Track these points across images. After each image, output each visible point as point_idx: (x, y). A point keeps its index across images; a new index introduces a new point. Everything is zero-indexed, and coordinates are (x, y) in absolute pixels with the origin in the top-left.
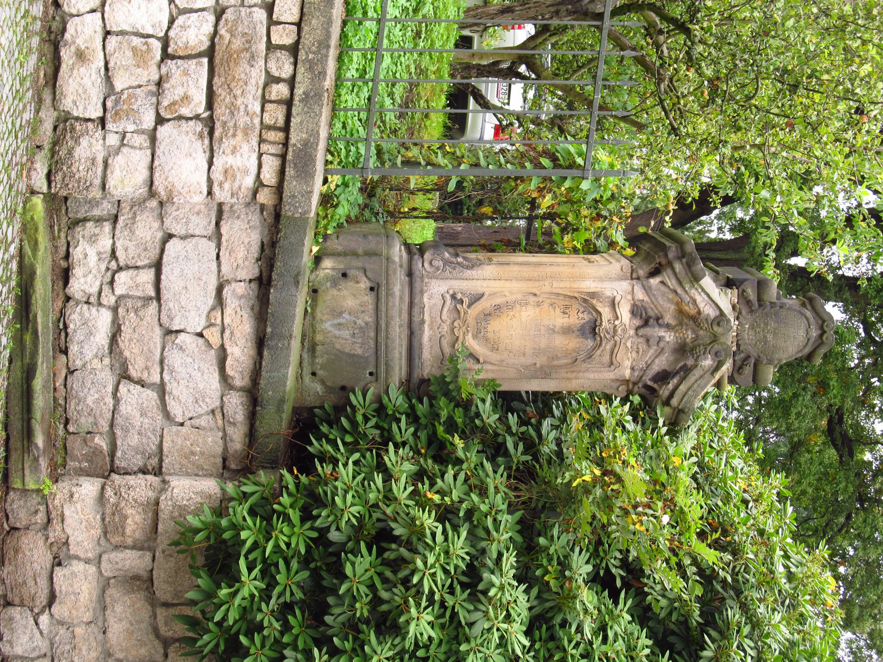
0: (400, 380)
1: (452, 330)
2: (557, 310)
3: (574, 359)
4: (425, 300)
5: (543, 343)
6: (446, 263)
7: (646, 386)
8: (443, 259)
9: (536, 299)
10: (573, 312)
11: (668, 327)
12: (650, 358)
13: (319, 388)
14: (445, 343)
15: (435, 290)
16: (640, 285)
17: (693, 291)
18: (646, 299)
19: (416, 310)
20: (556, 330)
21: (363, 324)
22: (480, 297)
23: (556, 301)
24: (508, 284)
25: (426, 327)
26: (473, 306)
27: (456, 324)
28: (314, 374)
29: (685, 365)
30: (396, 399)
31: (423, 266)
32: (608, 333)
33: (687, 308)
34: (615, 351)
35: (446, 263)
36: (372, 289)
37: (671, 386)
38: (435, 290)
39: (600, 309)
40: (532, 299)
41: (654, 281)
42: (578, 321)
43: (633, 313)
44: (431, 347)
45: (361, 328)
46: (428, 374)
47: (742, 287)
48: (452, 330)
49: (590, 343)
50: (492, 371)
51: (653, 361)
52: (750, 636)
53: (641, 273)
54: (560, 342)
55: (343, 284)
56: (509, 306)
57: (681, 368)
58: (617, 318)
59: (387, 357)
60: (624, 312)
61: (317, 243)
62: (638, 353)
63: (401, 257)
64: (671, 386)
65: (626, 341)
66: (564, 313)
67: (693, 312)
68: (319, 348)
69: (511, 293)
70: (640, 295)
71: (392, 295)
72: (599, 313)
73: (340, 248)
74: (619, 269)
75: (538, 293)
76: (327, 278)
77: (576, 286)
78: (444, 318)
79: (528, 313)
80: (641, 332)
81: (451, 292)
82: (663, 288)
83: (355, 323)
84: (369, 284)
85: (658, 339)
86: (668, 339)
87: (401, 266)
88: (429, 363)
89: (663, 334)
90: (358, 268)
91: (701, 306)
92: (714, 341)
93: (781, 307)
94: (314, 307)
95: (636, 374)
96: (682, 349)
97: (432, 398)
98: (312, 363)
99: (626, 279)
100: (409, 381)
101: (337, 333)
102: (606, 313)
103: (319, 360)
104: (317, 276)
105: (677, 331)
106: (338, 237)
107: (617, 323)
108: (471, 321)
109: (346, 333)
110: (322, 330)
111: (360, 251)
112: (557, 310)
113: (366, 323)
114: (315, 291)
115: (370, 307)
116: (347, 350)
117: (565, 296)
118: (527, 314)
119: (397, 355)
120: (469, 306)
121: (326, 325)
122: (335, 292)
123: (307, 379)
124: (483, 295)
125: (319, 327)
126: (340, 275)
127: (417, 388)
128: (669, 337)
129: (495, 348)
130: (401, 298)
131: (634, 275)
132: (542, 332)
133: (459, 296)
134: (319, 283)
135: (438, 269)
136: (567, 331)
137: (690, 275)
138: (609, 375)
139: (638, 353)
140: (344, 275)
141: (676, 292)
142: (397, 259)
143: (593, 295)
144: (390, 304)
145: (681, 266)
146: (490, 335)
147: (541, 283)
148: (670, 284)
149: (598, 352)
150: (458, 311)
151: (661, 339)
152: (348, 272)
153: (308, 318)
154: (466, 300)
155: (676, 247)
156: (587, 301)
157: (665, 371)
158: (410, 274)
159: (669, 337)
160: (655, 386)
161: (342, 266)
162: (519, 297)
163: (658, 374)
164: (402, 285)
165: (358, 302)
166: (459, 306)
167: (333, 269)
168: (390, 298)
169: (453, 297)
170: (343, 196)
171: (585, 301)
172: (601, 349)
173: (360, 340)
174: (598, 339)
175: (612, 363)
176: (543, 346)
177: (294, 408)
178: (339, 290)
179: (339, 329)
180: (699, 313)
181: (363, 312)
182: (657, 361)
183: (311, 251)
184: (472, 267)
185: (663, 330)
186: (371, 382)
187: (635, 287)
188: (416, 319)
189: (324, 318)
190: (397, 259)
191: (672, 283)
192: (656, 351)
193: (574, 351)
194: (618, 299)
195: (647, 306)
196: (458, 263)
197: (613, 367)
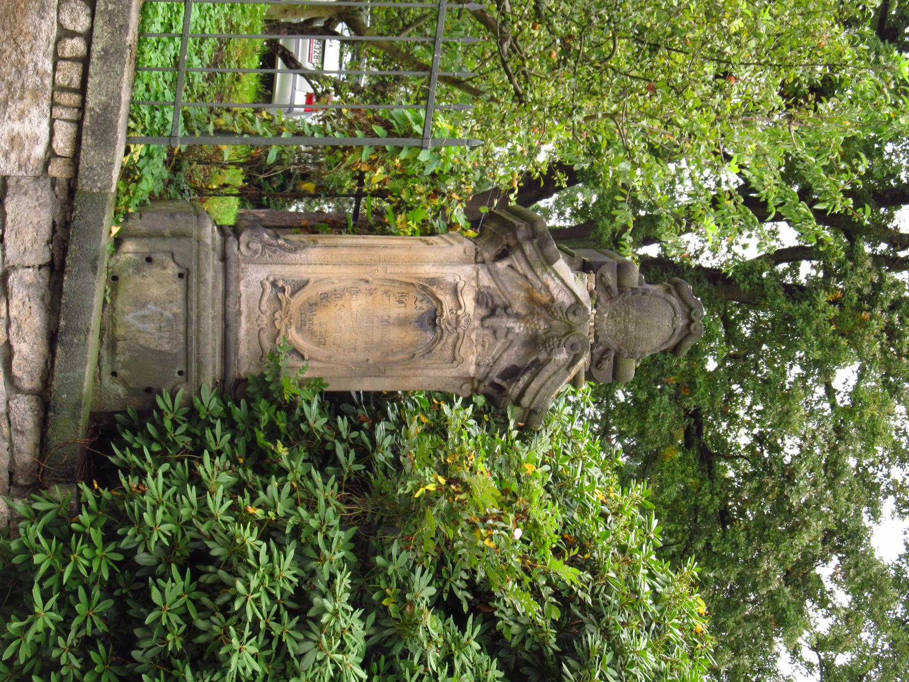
1: (273, 322)
2: (393, 299)
4: (242, 288)
5: (377, 336)
6: (265, 245)
8: (261, 241)
10: (410, 301)
11: (518, 317)
13: (120, 390)
16: (486, 270)
17: (546, 276)
18: (493, 285)
19: (231, 300)
20: (391, 321)
21: (171, 316)
24: (336, 270)
25: (243, 319)
27: (277, 315)
28: (114, 374)
29: (537, 360)
30: (209, 401)
33: (538, 295)
35: (265, 245)
36: (181, 276)
37: (521, 384)
39: (440, 297)
40: (364, 286)
41: (502, 265)
44: (249, 342)
45: (168, 320)
48: (273, 322)
49: (430, 336)
50: (319, 369)
53: (487, 255)
54: (396, 335)
55: (147, 270)
57: (533, 363)
58: (460, 307)
59: (198, 353)
60: (468, 301)
61: (117, 223)
62: (483, 346)
63: (213, 239)
64: (521, 384)
66: (400, 302)
67: (545, 299)
68: (120, 344)
69: (340, 279)
71: (205, 282)
73: (144, 229)
75: (370, 279)
76: (129, 263)
78: (264, 308)
80: (488, 322)
81: (271, 279)
82: (511, 273)
83: (162, 315)
84: (177, 270)
86: (517, 331)
87: (214, 249)
89: (512, 325)
90: (165, 252)
91: (555, 292)
93: (644, 293)
94: (114, 296)
95: (482, 370)
96: (533, 342)
97: (249, 400)
98: (112, 362)
100: (223, 380)
101: (141, 326)
102: (447, 301)
104: (117, 261)
106: (141, 216)
107: (460, 312)
109: (151, 327)
110: (124, 324)
111: (167, 233)
113: (175, 316)
114: (115, 278)
115: (179, 296)
116: (152, 346)
117: (401, 282)
118: (358, 303)
119: (210, 351)
120: (292, 295)
121: (129, 319)
122: (138, 279)
123: (107, 379)
124: (307, 282)
125: (119, 320)
127: (232, 389)
128: (519, 328)
130: (214, 286)
131: (479, 259)
132: (376, 324)
133: (280, 283)
134: (120, 269)
135: (256, 252)
136: (403, 322)
139: (483, 346)
140: (149, 260)
141: (526, 277)
142: (209, 241)
143: (433, 281)
144: (202, 293)
146: (316, 328)
147: (374, 268)
149: (439, 346)
150: (280, 301)
151: (509, 330)
152: (153, 256)
156: (426, 288)
158: (224, 258)
160: (504, 384)
161: (146, 250)
162: (349, 283)
164: (215, 271)
165: (164, 291)
166: (280, 295)
167: (136, 253)
168: (202, 286)
169: (274, 284)
170: (146, 168)
172: (442, 342)
173: (167, 335)
174: (439, 331)
176: (376, 338)
177: (91, 413)
178: (143, 277)
180: (552, 300)
181: (171, 302)
182: (505, 356)
184: (295, 250)
187: (481, 272)
188: (231, 310)
190: (209, 241)
191: (522, 267)
194: (461, 285)
195: (494, 293)
196: (279, 246)
197: (455, 363)
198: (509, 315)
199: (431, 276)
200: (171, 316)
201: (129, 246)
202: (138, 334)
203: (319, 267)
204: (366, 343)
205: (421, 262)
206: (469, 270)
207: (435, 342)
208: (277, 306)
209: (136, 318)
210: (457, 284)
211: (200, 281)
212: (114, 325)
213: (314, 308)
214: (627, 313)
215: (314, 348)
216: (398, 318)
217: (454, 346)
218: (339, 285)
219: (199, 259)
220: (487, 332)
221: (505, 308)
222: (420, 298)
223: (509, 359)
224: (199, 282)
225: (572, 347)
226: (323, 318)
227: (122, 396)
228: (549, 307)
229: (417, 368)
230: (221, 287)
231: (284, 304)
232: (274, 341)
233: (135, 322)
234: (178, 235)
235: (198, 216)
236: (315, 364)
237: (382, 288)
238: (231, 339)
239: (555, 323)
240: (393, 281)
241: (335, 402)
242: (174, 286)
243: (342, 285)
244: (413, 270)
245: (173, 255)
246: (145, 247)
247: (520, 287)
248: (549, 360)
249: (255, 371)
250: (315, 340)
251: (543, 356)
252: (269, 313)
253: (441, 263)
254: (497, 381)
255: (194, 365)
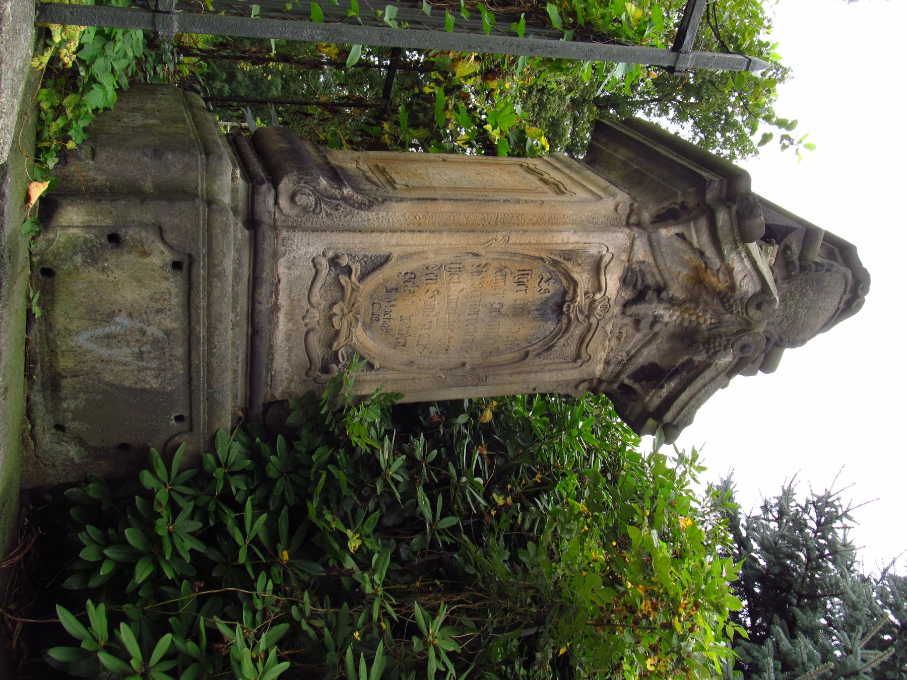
0: (234, 414)
1: (330, 318)
2: (510, 278)
3: (523, 352)
4: (282, 270)
5: (480, 333)
6: (321, 197)
7: (623, 386)
8: (315, 191)
9: (476, 261)
10: (533, 282)
11: (673, 303)
12: (634, 347)
13: (73, 451)
14: (315, 341)
15: (301, 252)
16: (645, 239)
17: (733, 255)
18: (649, 260)
19: (264, 291)
20: (503, 310)
21: (160, 334)
22: (383, 261)
23: (508, 264)
24: (434, 240)
25: (282, 317)
26: (370, 278)
27: (336, 309)
28: (60, 427)
29: (690, 361)
30: (232, 449)
31: (276, 203)
32: (581, 312)
33: (714, 280)
34: (587, 340)
35: (321, 197)
36: (176, 266)
37: (664, 392)
38: (301, 252)
39: (576, 276)
40: (471, 260)
41: (666, 233)
42: (538, 296)
43: (624, 281)
44: (290, 350)
45: (156, 341)
46: (283, 393)
47: (786, 241)
48: (330, 318)
49: (551, 326)
50: (395, 381)
51: (639, 351)
52: (226, 81)
53: (646, 216)
54: (507, 329)
55: (111, 259)
56: (430, 274)
57: (684, 365)
58: (599, 289)
59: (210, 386)
60: (612, 282)
61: (45, 174)
62: (619, 339)
63: (234, 191)
64: (664, 392)
65: (606, 323)
66: (519, 283)
67: (721, 284)
68: (67, 383)
69: (436, 252)
70: (641, 253)
71: (221, 276)
72: (576, 284)
73: (101, 179)
74: (612, 208)
75: (482, 252)
76: (74, 246)
77: (547, 241)
78: (315, 299)
79: (462, 285)
80: (633, 309)
81: (330, 254)
82: (678, 244)
83: (143, 333)
84: (169, 257)
85: (651, 319)
86: (666, 319)
87: (235, 211)
88: (285, 376)
89: (662, 312)
90: (144, 225)
91: (738, 277)
92: (743, 331)
93: (828, 270)
94: (48, 304)
95: (611, 368)
96: (687, 337)
97: (292, 436)
98: (55, 410)
99: (619, 226)
100: (248, 407)
101: (105, 352)
102: (583, 279)
103: (69, 405)
104: (50, 242)
105: (687, 310)
106: (94, 155)
107: (598, 296)
108: (363, 302)
109: (123, 353)
110: (71, 350)
111: (148, 185)
112: (510, 278)
113: (167, 333)
114: (48, 273)
115: (175, 301)
116: (127, 383)
117: (525, 256)
118: (460, 287)
119: (229, 376)
120: (361, 278)
121: (81, 342)
122: (94, 274)
123: (46, 439)
124: (387, 258)
125: (62, 345)
126: (104, 240)
127: (262, 420)
128: (669, 316)
129: (400, 344)
130: (236, 274)
131: (633, 219)
132: (481, 315)
133: (344, 261)
134: (56, 256)
135: (305, 209)
136: (520, 311)
137: (736, 231)
138: (573, 374)
139: (619, 339)
140: (114, 239)
141: (702, 254)
142: (227, 199)
143: (569, 255)
144: (216, 292)
145: (726, 217)
146: (394, 324)
147: (491, 236)
148: (695, 241)
149: (563, 340)
150: (342, 288)
151: (656, 320)
152: (121, 233)
153: (36, 326)
154: (356, 268)
155: (721, 183)
156: (559, 264)
157: (653, 365)
158: (252, 223)
159: (669, 316)
160: (636, 386)
161: (108, 222)
162: (449, 257)
163: (642, 369)
164: (238, 250)
165: (147, 293)
166: (343, 279)
167: (87, 227)
168: (216, 282)
169: (334, 261)
170: (100, 62)
171: (555, 263)
172: (567, 336)
173: (154, 364)
174: (565, 321)
175: (578, 356)
176: (479, 336)
177: (22, 491)
178: (104, 270)
179: (109, 346)
180: (732, 287)
181: (159, 311)
182: (645, 352)
183: (28, 198)
184: (369, 206)
185: (662, 306)
186: (179, 433)
187: (638, 243)
188: (264, 307)
189: (73, 327)
190: (227, 199)
191: (700, 237)
192: (645, 336)
193: (526, 340)
194: (607, 259)
195: (647, 270)
196: (344, 199)
197: (579, 362)
198: (660, 300)
199: (570, 247)
200: (160, 334)
201: (73, 218)
202: (99, 366)
203: (408, 235)
204: (464, 341)
205: (550, 224)
206: (621, 237)
207: (556, 335)
208: (337, 294)
209: (96, 339)
210: (601, 258)
211: (213, 273)
212: (53, 352)
213: (394, 295)
214: (803, 295)
215: (387, 351)
216: (514, 307)
217: (582, 340)
218: (433, 259)
219: (210, 236)
220: (627, 320)
221: (659, 290)
222: (546, 276)
223: (649, 355)
224: (210, 276)
225: (743, 348)
226: (410, 311)
227: (77, 460)
228: (726, 297)
229: (529, 372)
230: (246, 272)
231: (348, 293)
232: (330, 345)
233: (93, 346)
234: (174, 193)
235: (207, 155)
236: (389, 375)
237: (496, 264)
238: (263, 349)
239: (728, 317)
240: (515, 254)
241: (405, 418)
242: (165, 285)
243: (439, 259)
244: (547, 239)
245: (161, 231)
246: (104, 217)
247: (683, 263)
248: (707, 365)
249: (299, 389)
250: (391, 340)
251: (699, 358)
252: (324, 304)
253: (585, 227)
254: (627, 381)
255: (202, 407)
